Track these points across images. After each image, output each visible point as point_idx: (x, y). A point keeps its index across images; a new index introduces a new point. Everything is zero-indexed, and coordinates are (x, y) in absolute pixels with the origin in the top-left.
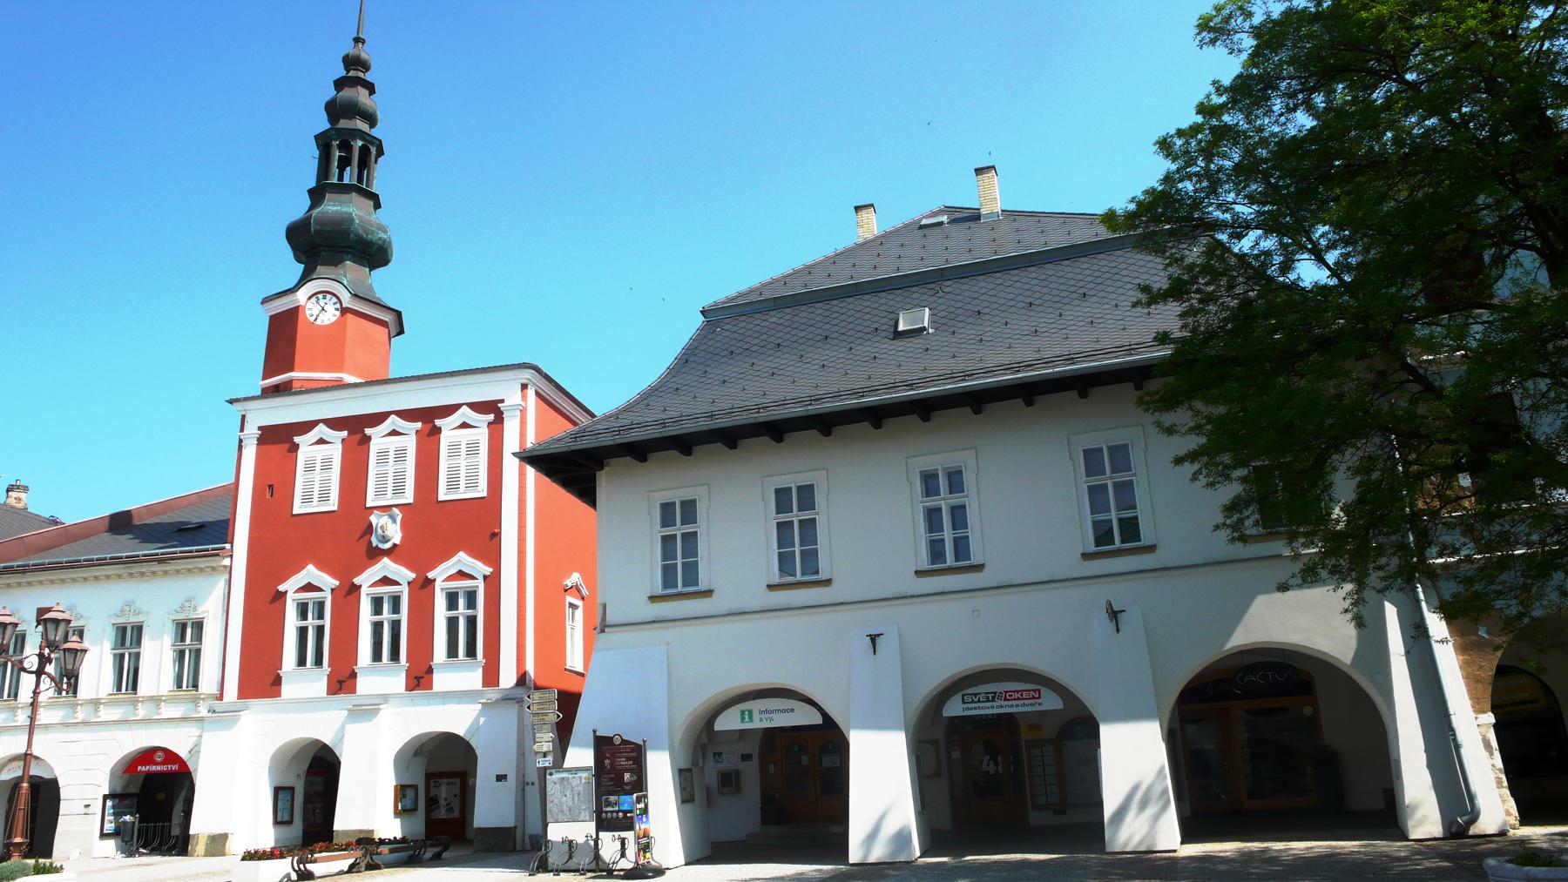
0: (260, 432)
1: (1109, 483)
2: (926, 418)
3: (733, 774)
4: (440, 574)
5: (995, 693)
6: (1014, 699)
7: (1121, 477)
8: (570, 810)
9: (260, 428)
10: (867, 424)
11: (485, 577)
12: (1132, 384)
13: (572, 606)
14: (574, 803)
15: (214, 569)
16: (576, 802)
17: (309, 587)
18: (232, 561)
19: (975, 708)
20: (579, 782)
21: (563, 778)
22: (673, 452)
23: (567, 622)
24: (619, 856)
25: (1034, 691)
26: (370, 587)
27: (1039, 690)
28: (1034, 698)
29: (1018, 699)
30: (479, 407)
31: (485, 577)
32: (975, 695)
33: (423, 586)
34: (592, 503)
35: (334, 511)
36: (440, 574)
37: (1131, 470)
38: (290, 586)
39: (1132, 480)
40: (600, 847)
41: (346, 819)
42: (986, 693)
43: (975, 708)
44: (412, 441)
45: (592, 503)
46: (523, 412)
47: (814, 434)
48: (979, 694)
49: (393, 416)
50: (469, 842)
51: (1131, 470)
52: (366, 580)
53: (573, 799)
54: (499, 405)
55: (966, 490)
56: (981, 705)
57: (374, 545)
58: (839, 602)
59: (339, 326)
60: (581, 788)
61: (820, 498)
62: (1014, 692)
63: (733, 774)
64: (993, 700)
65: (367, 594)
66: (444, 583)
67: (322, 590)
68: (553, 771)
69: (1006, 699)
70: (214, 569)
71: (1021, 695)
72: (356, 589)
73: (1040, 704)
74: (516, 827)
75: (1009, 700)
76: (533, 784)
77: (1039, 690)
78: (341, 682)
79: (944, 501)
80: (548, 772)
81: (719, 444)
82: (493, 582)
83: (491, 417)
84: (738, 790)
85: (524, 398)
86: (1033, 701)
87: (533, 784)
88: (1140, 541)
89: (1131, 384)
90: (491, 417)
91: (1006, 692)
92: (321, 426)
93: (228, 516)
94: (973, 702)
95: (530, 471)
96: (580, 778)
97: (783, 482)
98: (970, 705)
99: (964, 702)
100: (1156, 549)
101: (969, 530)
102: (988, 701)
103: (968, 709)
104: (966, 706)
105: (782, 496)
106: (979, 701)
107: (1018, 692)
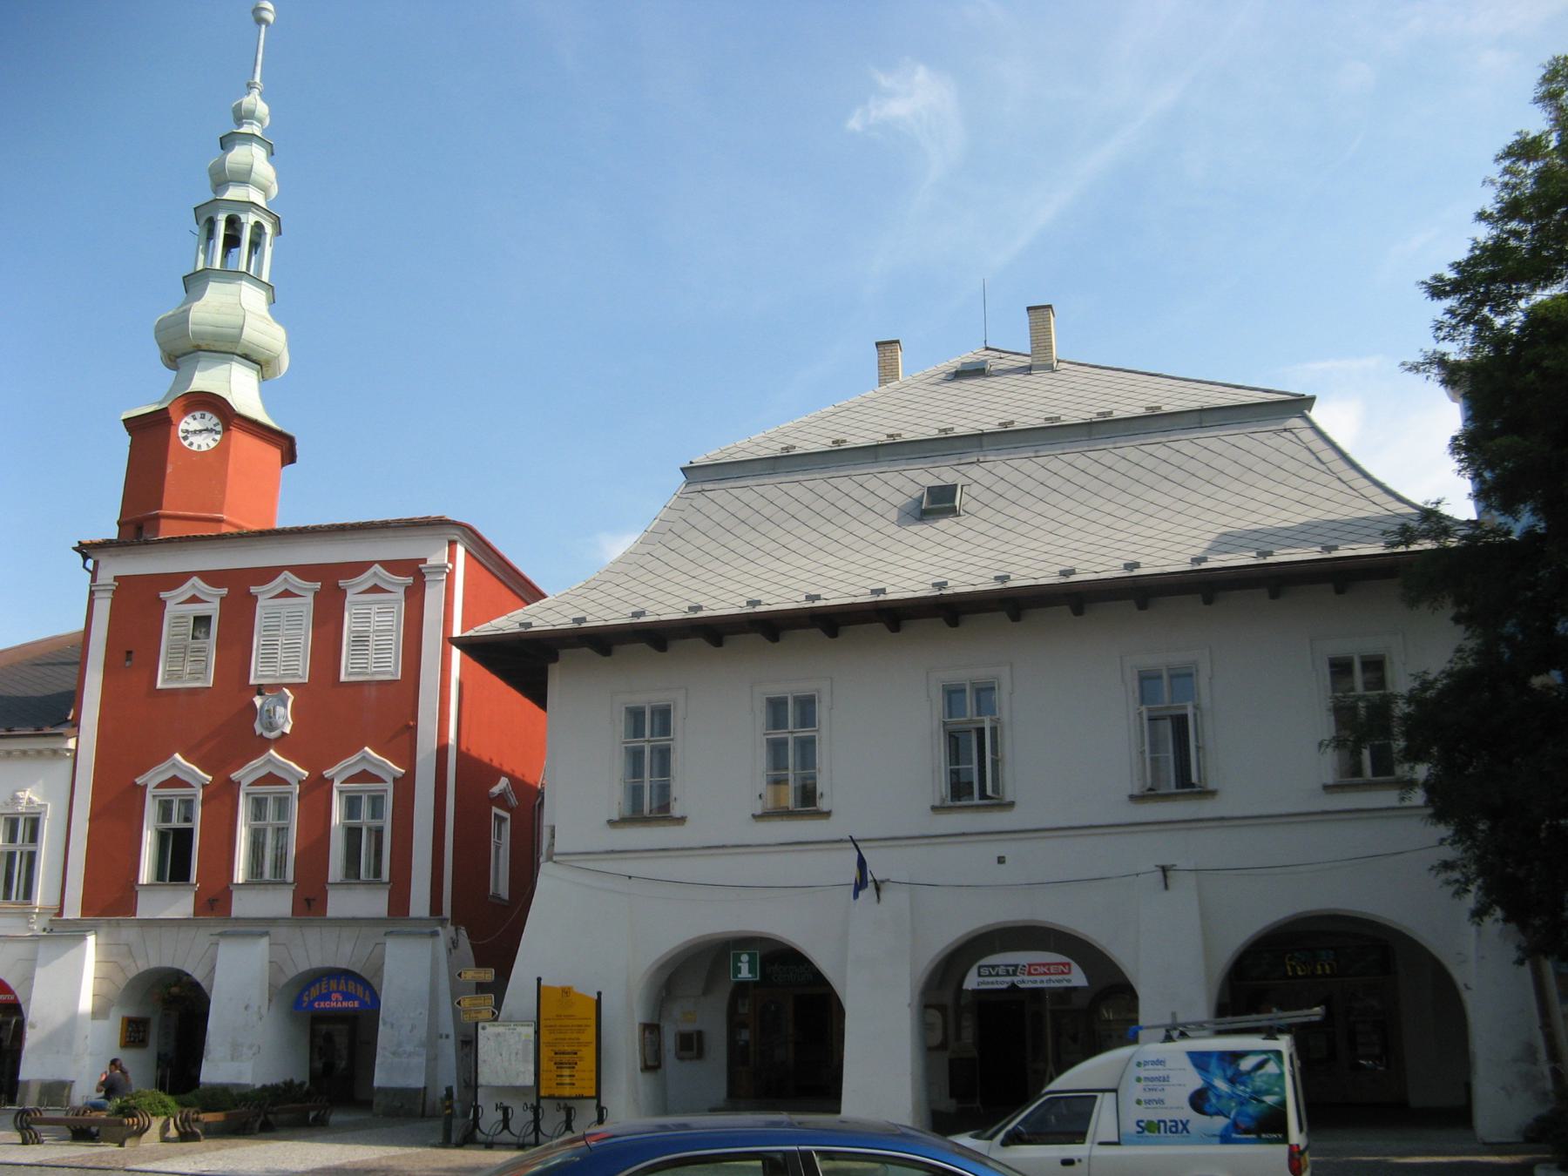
0: (117, 584)
1: (790, 738)
2: (1016, 617)
3: (695, 1036)
4: (338, 773)
5: (1016, 966)
6: (1041, 974)
7: (805, 733)
8: (505, 1071)
9: (116, 578)
10: (1004, 615)
11: (204, 786)
12: (1199, 595)
13: (501, 819)
14: (511, 1064)
15: (55, 752)
16: (513, 1062)
17: (175, 782)
18: (77, 741)
19: (992, 983)
20: (517, 1039)
21: (499, 1034)
22: (586, 650)
23: (492, 839)
24: (564, 1129)
25: (1064, 964)
26: (249, 785)
27: (1069, 964)
28: (1063, 973)
29: (1045, 974)
30: (393, 566)
31: (395, 780)
32: (993, 967)
33: (316, 790)
34: (540, 699)
35: (305, 683)
36: (338, 773)
37: (815, 726)
38: (151, 779)
39: (815, 736)
40: (510, 1116)
41: (216, 1069)
42: (1006, 966)
43: (992, 983)
44: (310, 604)
45: (540, 699)
46: (451, 577)
47: (880, 627)
48: (998, 966)
49: (286, 572)
50: (366, 1105)
51: (815, 726)
52: (246, 775)
53: (510, 1060)
54: (421, 566)
55: (672, 734)
56: (999, 979)
57: (258, 733)
58: (721, 844)
59: (222, 450)
60: (520, 1046)
61: (821, 712)
62: (1039, 965)
63: (695, 1036)
64: (1014, 974)
65: (154, 796)
66: (249, 787)
67: (190, 786)
68: (487, 1024)
69: (1030, 974)
70: (55, 752)
71: (1049, 969)
72: (233, 787)
73: (1069, 981)
74: (425, 1088)
75: (1034, 975)
76: (447, 1037)
77: (1069, 964)
78: (308, 901)
79: (791, 733)
80: (480, 1025)
81: (759, 635)
82: (405, 786)
83: (410, 580)
84: (700, 1054)
85: (452, 558)
86: (1060, 977)
87: (447, 1037)
88: (360, 819)
89: (1199, 596)
90: (410, 580)
91: (1030, 965)
92: (195, 579)
93: (70, 685)
94: (990, 975)
95: (456, 653)
96: (520, 1034)
97: (777, 690)
98: (986, 979)
99: (980, 975)
100: (685, 821)
101: (671, 778)
102: (1008, 974)
103: (983, 983)
104: (981, 979)
105: (776, 707)
106: (997, 975)
107: (1044, 965)
